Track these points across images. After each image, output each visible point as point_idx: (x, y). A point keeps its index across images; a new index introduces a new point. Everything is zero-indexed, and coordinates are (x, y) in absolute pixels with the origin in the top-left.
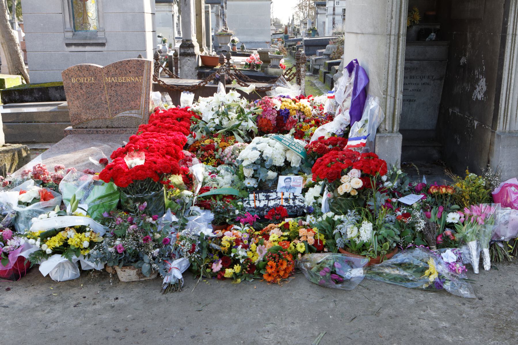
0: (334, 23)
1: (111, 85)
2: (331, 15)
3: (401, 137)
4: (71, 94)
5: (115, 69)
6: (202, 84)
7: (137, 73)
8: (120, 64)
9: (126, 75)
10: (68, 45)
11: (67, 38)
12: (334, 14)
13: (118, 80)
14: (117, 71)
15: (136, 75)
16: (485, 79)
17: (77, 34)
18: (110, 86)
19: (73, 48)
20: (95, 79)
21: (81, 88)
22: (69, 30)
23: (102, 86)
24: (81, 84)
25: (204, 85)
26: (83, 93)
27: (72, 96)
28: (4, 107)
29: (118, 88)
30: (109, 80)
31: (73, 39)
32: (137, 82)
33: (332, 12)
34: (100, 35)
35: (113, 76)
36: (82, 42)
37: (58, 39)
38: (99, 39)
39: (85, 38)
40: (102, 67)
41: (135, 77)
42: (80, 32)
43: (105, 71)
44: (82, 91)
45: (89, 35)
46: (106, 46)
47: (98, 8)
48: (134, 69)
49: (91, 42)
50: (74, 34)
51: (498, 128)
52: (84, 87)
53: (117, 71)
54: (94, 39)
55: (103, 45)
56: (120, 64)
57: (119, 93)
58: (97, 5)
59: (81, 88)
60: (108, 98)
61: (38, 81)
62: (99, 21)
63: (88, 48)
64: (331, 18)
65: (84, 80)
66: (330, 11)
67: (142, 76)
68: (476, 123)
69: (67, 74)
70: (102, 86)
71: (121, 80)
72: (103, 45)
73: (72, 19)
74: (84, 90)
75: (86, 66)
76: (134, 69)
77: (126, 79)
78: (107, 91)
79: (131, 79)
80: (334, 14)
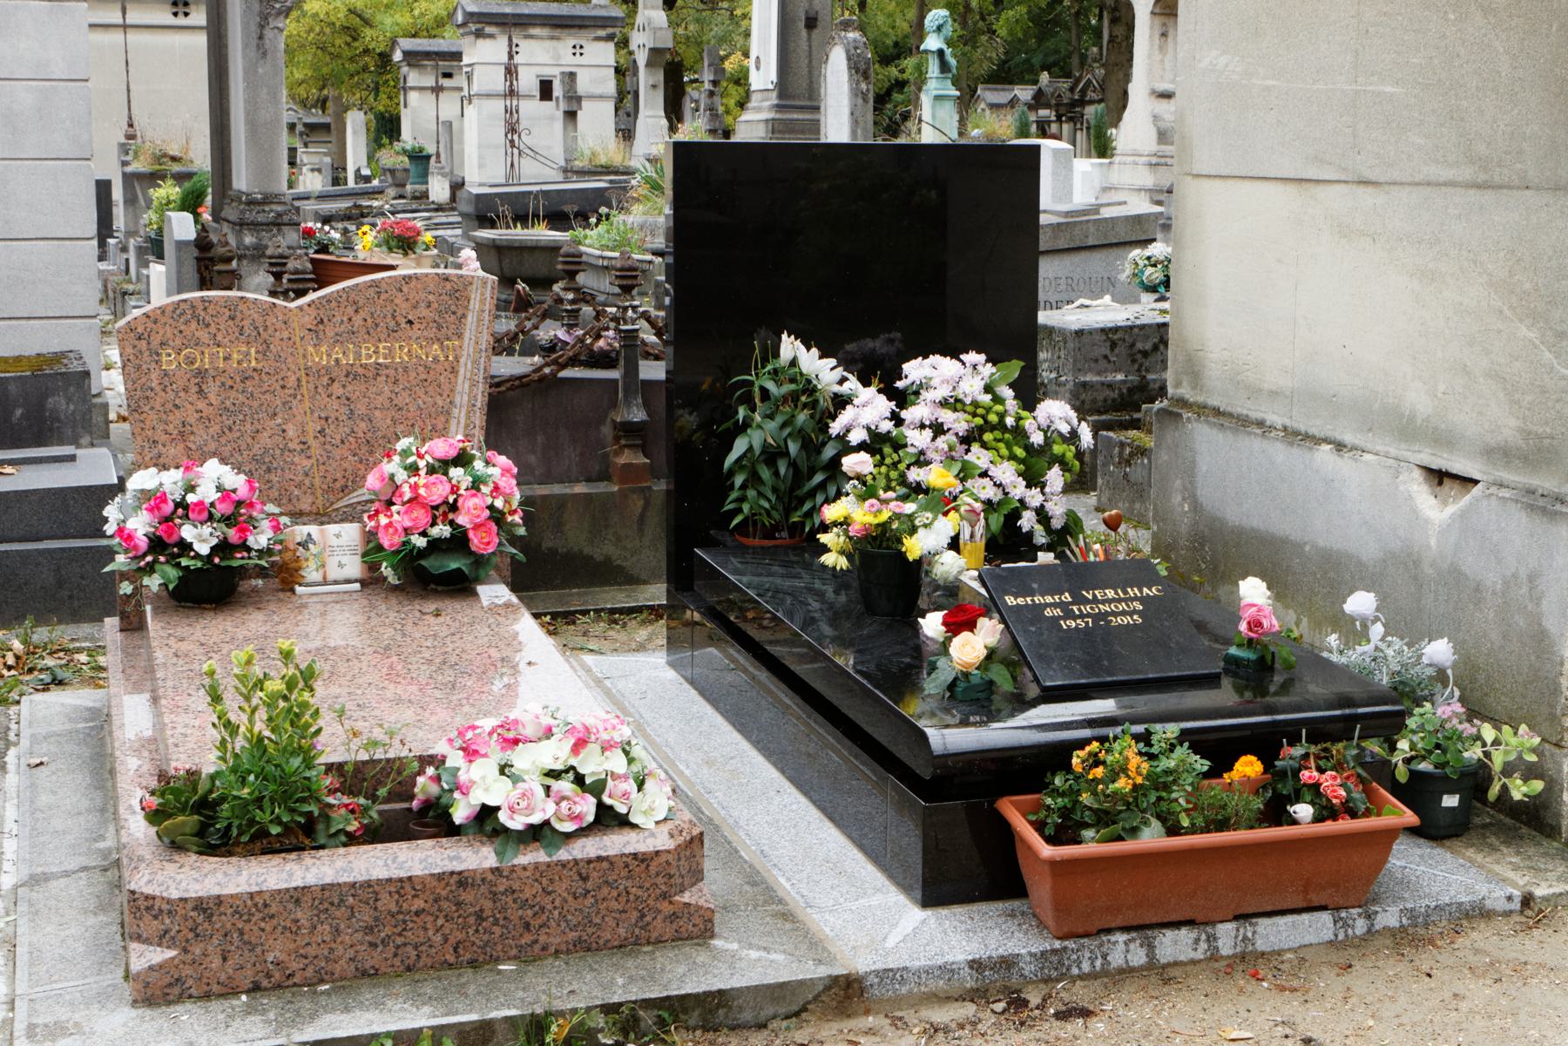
0: (512, 129)
5: (350, 310)
7: (439, 328)
8: (372, 291)
12: (512, 93)
13: (358, 356)
18: (325, 380)
21: (200, 391)
24: (201, 373)
26: (208, 411)
29: (355, 389)
30: (320, 356)
32: (436, 360)
35: (337, 340)
44: (201, 405)
48: (424, 312)
52: (212, 388)
56: (372, 291)
57: (361, 408)
59: (200, 391)
60: (313, 427)
64: (498, 106)
66: (494, 79)
67: (460, 336)
71: (370, 354)
74: (212, 398)
76: (424, 312)
78: (312, 398)
80: (512, 93)
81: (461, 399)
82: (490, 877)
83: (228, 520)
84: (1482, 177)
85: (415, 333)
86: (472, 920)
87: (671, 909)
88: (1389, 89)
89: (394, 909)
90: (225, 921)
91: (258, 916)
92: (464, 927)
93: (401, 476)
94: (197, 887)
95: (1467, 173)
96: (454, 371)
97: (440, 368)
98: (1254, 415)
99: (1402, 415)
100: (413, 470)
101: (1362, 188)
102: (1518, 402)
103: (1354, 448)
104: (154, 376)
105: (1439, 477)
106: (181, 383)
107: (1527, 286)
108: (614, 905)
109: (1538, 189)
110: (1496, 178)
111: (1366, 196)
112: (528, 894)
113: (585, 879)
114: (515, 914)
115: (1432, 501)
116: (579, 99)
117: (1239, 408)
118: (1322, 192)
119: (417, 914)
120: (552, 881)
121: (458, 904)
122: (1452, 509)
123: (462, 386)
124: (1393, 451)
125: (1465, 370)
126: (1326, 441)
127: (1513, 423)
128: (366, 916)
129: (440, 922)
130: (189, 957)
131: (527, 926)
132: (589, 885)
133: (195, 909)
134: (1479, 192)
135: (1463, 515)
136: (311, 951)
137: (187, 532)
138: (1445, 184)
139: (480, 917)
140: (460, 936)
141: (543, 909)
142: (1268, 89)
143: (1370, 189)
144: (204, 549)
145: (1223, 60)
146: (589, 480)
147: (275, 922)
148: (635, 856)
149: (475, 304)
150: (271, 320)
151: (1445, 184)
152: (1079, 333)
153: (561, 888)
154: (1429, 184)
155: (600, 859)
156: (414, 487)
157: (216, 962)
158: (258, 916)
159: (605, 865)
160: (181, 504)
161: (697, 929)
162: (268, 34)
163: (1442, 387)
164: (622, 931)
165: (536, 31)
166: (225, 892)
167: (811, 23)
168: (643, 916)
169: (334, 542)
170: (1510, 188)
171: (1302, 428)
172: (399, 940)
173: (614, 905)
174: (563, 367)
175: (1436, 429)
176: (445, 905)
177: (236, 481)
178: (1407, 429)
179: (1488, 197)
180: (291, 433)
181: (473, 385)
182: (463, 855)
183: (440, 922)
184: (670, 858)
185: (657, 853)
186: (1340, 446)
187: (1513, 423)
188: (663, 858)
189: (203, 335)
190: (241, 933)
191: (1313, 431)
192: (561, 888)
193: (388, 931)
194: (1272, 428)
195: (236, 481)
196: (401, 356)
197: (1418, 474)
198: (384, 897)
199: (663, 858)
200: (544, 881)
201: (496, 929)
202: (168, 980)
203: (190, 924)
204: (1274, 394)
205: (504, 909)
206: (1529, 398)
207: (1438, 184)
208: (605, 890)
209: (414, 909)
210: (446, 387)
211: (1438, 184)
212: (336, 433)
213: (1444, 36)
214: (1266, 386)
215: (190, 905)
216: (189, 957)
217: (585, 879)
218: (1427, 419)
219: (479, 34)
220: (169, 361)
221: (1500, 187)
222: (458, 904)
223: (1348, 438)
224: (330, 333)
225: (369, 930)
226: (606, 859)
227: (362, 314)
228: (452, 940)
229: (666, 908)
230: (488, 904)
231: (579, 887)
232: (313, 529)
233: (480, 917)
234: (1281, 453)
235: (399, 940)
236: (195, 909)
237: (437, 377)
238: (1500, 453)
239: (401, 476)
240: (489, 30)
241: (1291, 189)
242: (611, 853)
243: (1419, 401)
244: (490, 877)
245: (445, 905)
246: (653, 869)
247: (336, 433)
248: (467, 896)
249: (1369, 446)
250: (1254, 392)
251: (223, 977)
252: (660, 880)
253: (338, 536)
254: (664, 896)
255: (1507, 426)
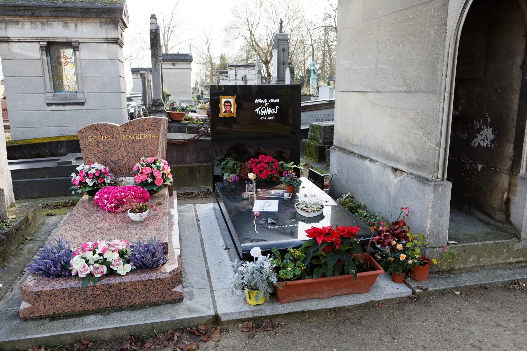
1: (128, 142)
2: (233, 80)
3: (451, 185)
4: (87, 152)
5: (132, 127)
6: (196, 138)
7: (154, 130)
8: (137, 122)
9: (143, 132)
10: (49, 104)
11: (48, 99)
12: (236, 80)
13: (135, 137)
14: (134, 129)
15: (152, 132)
16: (491, 129)
17: (57, 95)
18: (127, 143)
19: (54, 107)
20: (112, 137)
21: (98, 146)
22: (49, 91)
23: (119, 143)
24: (98, 142)
25: (198, 139)
26: (100, 150)
27: (89, 154)
28: (10, 164)
29: (135, 145)
30: (126, 137)
31: (53, 100)
32: (154, 138)
33: (234, 78)
34: (80, 95)
36: (62, 102)
37: (40, 100)
38: (79, 99)
39: (66, 98)
40: (118, 125)
41: (152, 134)
42: (60, 93)
43: (123, 129)
44: (98, 149)
45: (68, 96)
46: (85, 106)
47: (77, 72)
48: (150, 127)
49: (72, 102)
50: (54, 95)
51: (521, 172)
52: (101, 145)
53: (134, 129)
54: (74, 99)
55: (82, 104)
56: (137, 122)
57: (136, 150)
58: (76, 69)
59: (98, 146)
60: (125, 154)
61: (20, 138)
62: (78, 83)
63: (68, 107)
65: (101, 138)
67: (159, 132)
68: (480, 167)
69: (84, 132)
70: (119, 143)
72: (82, 104)
73: (52, 82)
74: (101, 147)
75: (103, 124)
76: (150, 127)
77: (143, 136)
78: (125, 147)
79: (147, 136)
80: (236, 80)
81: (160, 147)
82: (118, 285)
83: (98, 178)
84: (408, 89)
85: (148, 132)
86: (114, 296)
87: (170, 293)
88: (385, 67)
89: (92, 294)
90: (44, 297)
91: (53, 296)
92: (112, 298)
93: (140, 167)
94: (36, 288)
95: (404, 88)
96: (158, 141)
97: (155, 140)
98: (352, 151)
99: (386, 153)
100: (143, 165)
101: (378, 94)
102: (416, 151)
103: (374, 161)
104: (87, 142)
105: (395, 170)
106: (93, 144)
107: (420, 119)
108: (154, 292)
109: (424, 92)
110: (412, 90)
111: (379, 96)
112: (129, 289)
113: (145, 285)
114: (126, 295)
115: (394, 176)
116: (247, 80)
117: (349, 148)
118: (369, 95)
119: (98, 295)
120: (136, 286)
121: (110, 292)
122: (399, 179)
123: (160, 144)
124: (384, 162)
125: (403, 142)
126: (368, 158)
127: (415, 157)
128: (84, 295)
129: (105, 297)
130: (35, 307)
131: (130, 297)
132: (147, 287)
133: (35, 294)
134: (407, 94)
135: (401, 181)
136: (69, 305)
137: (87, 180)
138: (398, 92)
139: (116, 295)
140: (111, 300)
141: (134, 293)
142: (356, 69)
143: (379, 94)
144: (91, 184)
145: (346, 62)
146: (207, 162)
147: (58, 297)
148: (159, 279)
149: (162, 125)
150: (114, 129)
151: (398, 92)
152: (325, 127)
153: (139, 288)
154: (394, 92)
155: (149, 280)
156: (142, 169)
157: (43, 308)
158: (53, 296)
159: (151, 282)
160: (87, 174)
161: (178, 300)
162: (157, 66)
163: (396, 146)
164: (157, 298)
165: (241, 68)
166: (43, 290)
167: (284, 64)
168: (162, 295)
169: (128, 181)
170: (415, 92)
171: (363, 155)
172: (94, 302)
173: (154, 292)
174: (200, 137)
175: (395, 157)
176: (106, 292)
177: (101, 167)
178: (388, 157)
179: (410, 95)
180: (120, 156)
181: (163, 144)
182: (111, 279)
183: (105, 297)
184: (169, 280)
185: (166, 278)
186: (371, 160)
187: (415, 157)
188: (167, 280)
189: (98, 133)
190: (49, 300)
191: (365, 155)
192: (139, 288)
193: (90, 299)
194: (356, 154)
195: (101, 167)
196: (145, 137)
197: (390, 169)
198: (89, 290)
199: (167, 280)
200: (134, 286)
201: (121, 299)
202: (29, 312)
203: (34, 298)
204: (356, 145)
205: (123, 293)
206: (419, 151)
207: (397, 92)
208: (151, 288)
209: (97, 293)
210: (156, 144)
211: (397, 92)
212: (130, 155)
213: (399, 51)
214: (355, 144)
215: (34, 293)
216: (35, 307)
217: (145, 285)
218: (392, 155)
219: (231, 69)
220: (90, 139)
221: (413, 92)
222: (110, 292)
223: (373, 158)
224: (128, 132)
225: (85, 299)
226: (151, 280)
227: (135, 128)
228: (109, 301)
229: (168, 292)
230: (118, 292)
231: (144, 287)
232: (123, 178)
233: (116, 295)
234: (357, 160)
235: (94, 302)
236: (35, 294)
237: (154, 143)
238: (411, 165)
239: (140, 167)
240: (233, 68)
241: (361, 94)
242: (152, 278)
243: (390, 150)
244: (118, 285)
245: (106, 292)
246: (165, 283)
247: (130, 155)
248: (112, 290)
249: (378, 160)
250: (352, 145)
251: (45, 311)
252: (167, 285)
253: (129, 180)
254: (168, 289)
255: (414, 158)
